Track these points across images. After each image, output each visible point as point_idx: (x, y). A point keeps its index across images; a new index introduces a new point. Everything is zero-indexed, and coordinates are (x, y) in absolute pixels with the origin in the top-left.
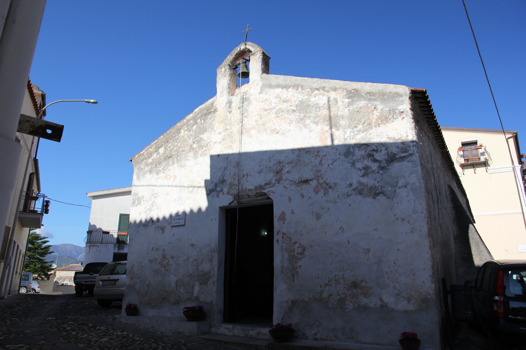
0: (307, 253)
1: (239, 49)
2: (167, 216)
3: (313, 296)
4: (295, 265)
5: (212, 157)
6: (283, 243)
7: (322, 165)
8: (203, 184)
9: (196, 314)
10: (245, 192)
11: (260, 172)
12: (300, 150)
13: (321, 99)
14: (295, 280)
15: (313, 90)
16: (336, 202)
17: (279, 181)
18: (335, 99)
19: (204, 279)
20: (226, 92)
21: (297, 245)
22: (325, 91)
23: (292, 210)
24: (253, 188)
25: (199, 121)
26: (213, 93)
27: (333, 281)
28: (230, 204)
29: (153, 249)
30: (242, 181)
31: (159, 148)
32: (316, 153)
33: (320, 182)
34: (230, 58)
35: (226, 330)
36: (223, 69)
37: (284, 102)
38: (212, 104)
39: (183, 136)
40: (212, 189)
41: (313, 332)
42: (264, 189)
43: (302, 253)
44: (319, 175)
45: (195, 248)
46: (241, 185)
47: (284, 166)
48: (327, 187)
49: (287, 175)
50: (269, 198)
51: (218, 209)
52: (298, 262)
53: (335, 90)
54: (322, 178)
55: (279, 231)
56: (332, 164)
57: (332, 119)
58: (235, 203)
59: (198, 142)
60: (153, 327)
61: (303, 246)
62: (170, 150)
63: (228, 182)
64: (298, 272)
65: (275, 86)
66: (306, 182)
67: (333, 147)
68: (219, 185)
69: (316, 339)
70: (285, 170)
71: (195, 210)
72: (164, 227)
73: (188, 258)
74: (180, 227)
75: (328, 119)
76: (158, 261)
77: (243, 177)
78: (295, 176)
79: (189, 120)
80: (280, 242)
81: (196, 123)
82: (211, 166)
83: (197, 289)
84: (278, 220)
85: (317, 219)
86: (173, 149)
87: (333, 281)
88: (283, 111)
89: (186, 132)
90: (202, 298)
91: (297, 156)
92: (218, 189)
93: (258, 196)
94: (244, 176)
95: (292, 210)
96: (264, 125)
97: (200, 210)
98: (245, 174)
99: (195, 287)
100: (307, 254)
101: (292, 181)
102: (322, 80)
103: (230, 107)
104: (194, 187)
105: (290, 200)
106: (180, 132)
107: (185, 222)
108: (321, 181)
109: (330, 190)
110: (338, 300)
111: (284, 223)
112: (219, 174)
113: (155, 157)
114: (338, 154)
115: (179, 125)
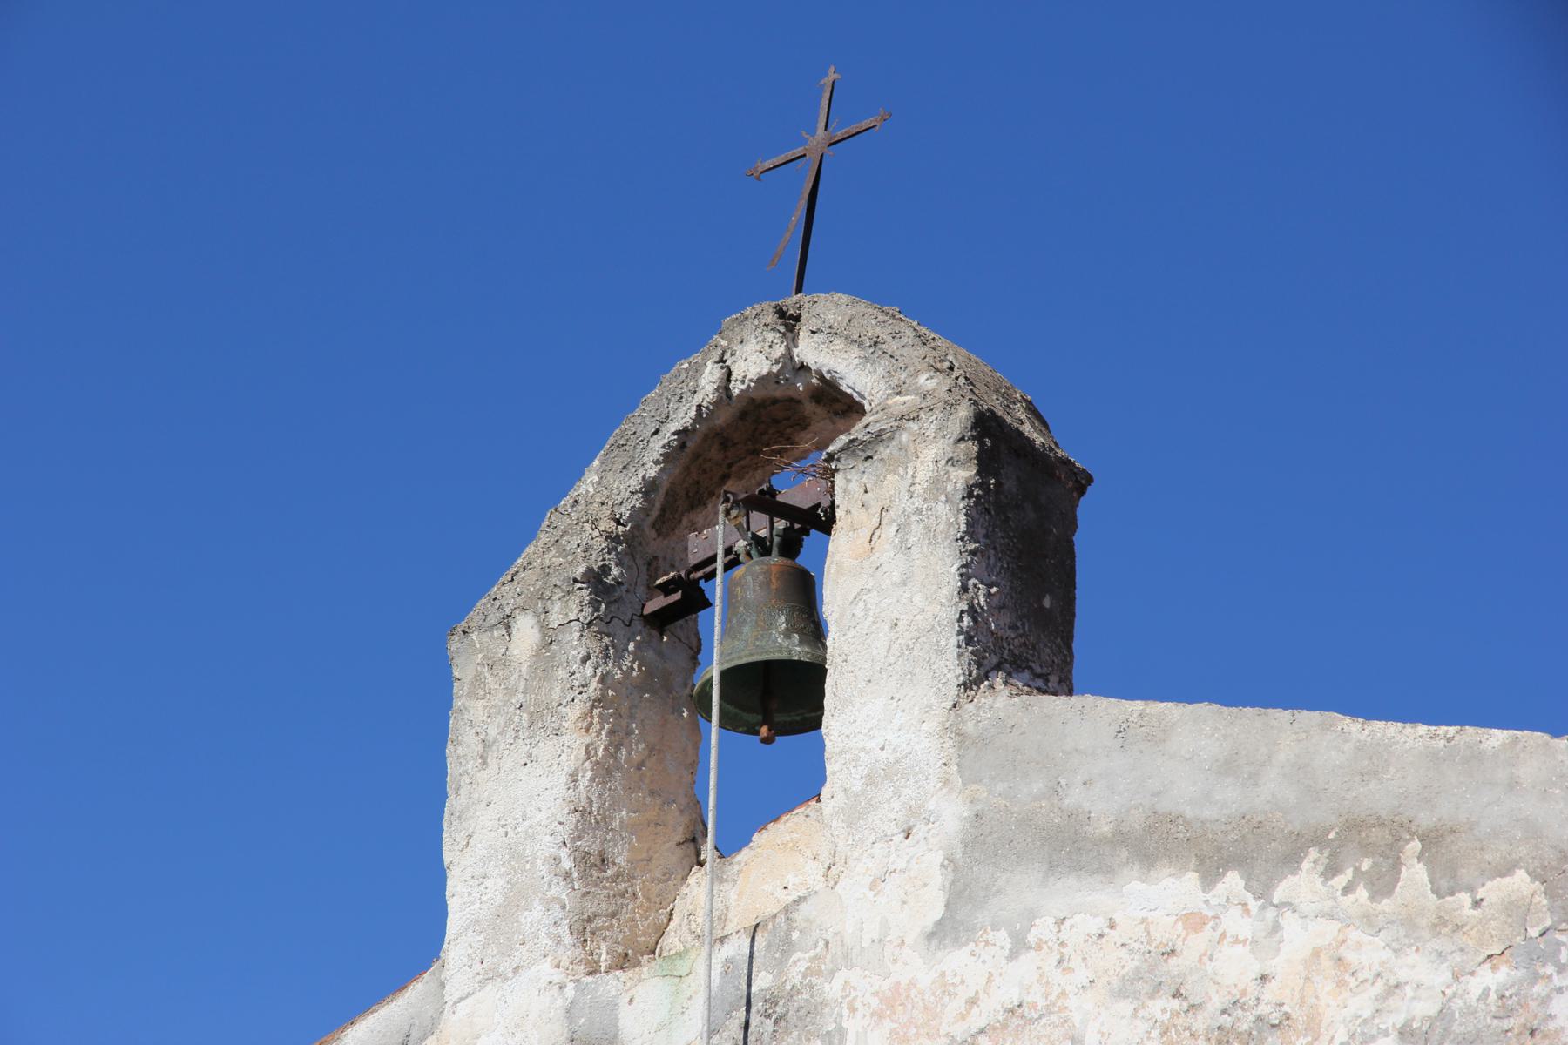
1: (710, 378)
20: (544, 919)
36: (526, 631)
65: (1120, 838)
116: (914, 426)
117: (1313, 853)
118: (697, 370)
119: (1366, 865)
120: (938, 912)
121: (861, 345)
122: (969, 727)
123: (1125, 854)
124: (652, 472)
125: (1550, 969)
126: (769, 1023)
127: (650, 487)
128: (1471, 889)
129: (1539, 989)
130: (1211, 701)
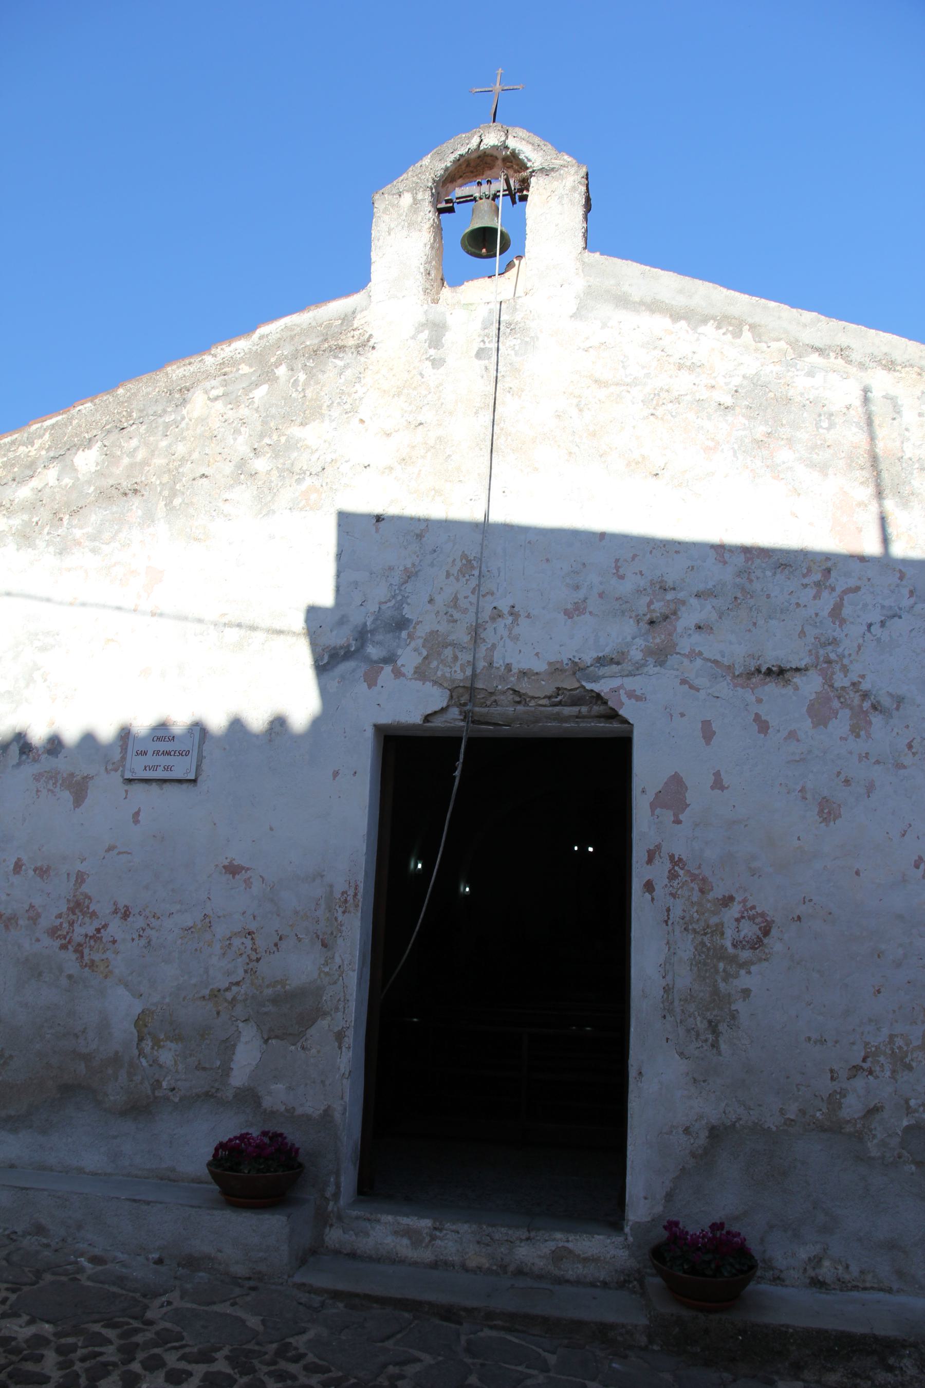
0: (775, 944)
1: (475, 141)
2: (106, 731)
3: (803, 1112)
4: (722, 986)
5: (347, 522)
6: (673, 895)
7: (843, 622)
8: (298, 622)
9: (257, 1171)
10: (503, 679)
11: (575, 611)
12: (752, 555)
13: (841, 391)
14: (723, 1047)
15: (801, 349)
16: (900, 766)
17: (661, 655)
18: (892, 400)
19: (289, 1015)
20: (415, 282)
21: (735, 910)
22: (849, 362)
23: (717, 774)
24: (540, 666)
25: (282, 371)
26: (353, 275)
27: (882, 1059)
28: (427, 718)
29: (18, 867)
30: (489, 635)
31: (73, 448)
32: (817, 577)
33: (837, 684)
34: (434, 165)
35: (396, 1236)
36: (407, 199)
37: (680, 367)
38: (347, 319)
39: (202, 420)
40: (339, 647)
41: (804, 1253)
42: (596, 679)
43: (756, 944)
44: (833, 656)
45: (248, 883)
46: (482, 650)
47: (684, 603)
48: (866, 705)
49: (697, 637)
50: (613, 715)
51: (370, 733)
52: (737, 976)
53: (890, 365)
54: (845, 670)
55: (659, 847)
56: (883, 624)
57: (882, 466)
58: (453, 719)
59: (277, 451)
60: (40, 1230)
61: (763, 915)
62: (132, 466)
63: (422, 631)
64: (734, 1016)
65: (642, 303)
66: (779, 673)
67: (886, 564)
68: (379, 637)
69: (817, 1283)
70: (687, 619)
71: (257, 720)
72: (87, 778)
73: (208, 922)
74: (166, 787)
75: (863, 459)
76: (46, 922)
77: (493, 619)
78: (733, 645)
79: (234, 362)
80: (659, 891)
81: (267, 376)
82: (339, 556)
83: (247, 1057)
84: (653, 806)
85: (825, 820)
86: (145, 463)
87: (882, 1059)
88: (677, 400)
89: (219, 405)
90: (276, 1096)
91: (739, 574)
92: (373, 651)
93: (559, 704)
94: (497, 614)
95: (717, 774)
96: (594, 434)
97: (279, 724)
98: (506, 611)
99: (240, 1048)
100: (778, 947)
101: (715, 662)
102: (835, 324)
103: (436, 342)
104: (253, 628)
105: (708, 733)
106: (185, 401)
107: (198, 767)
108: (840, 681)
109: (877, 720)
110: (908, 1129)
111: (678, 822)
112: (380, 592)
113: (52, 481)
114: (905, 592)
115: (177, 372)
116: (566, 169)
117: (712, 322)
118: (470, 138)
119: (731, 328)
120: (574, 310)
121: (533, 145)
122: (586, 260)
123: (644, 308)
124: (449, 165)
125: (793, 369)
126: (508, 330)
127: (447, 169)
128: (766, 342)
129: (790, 374)
130: (674, 272)
